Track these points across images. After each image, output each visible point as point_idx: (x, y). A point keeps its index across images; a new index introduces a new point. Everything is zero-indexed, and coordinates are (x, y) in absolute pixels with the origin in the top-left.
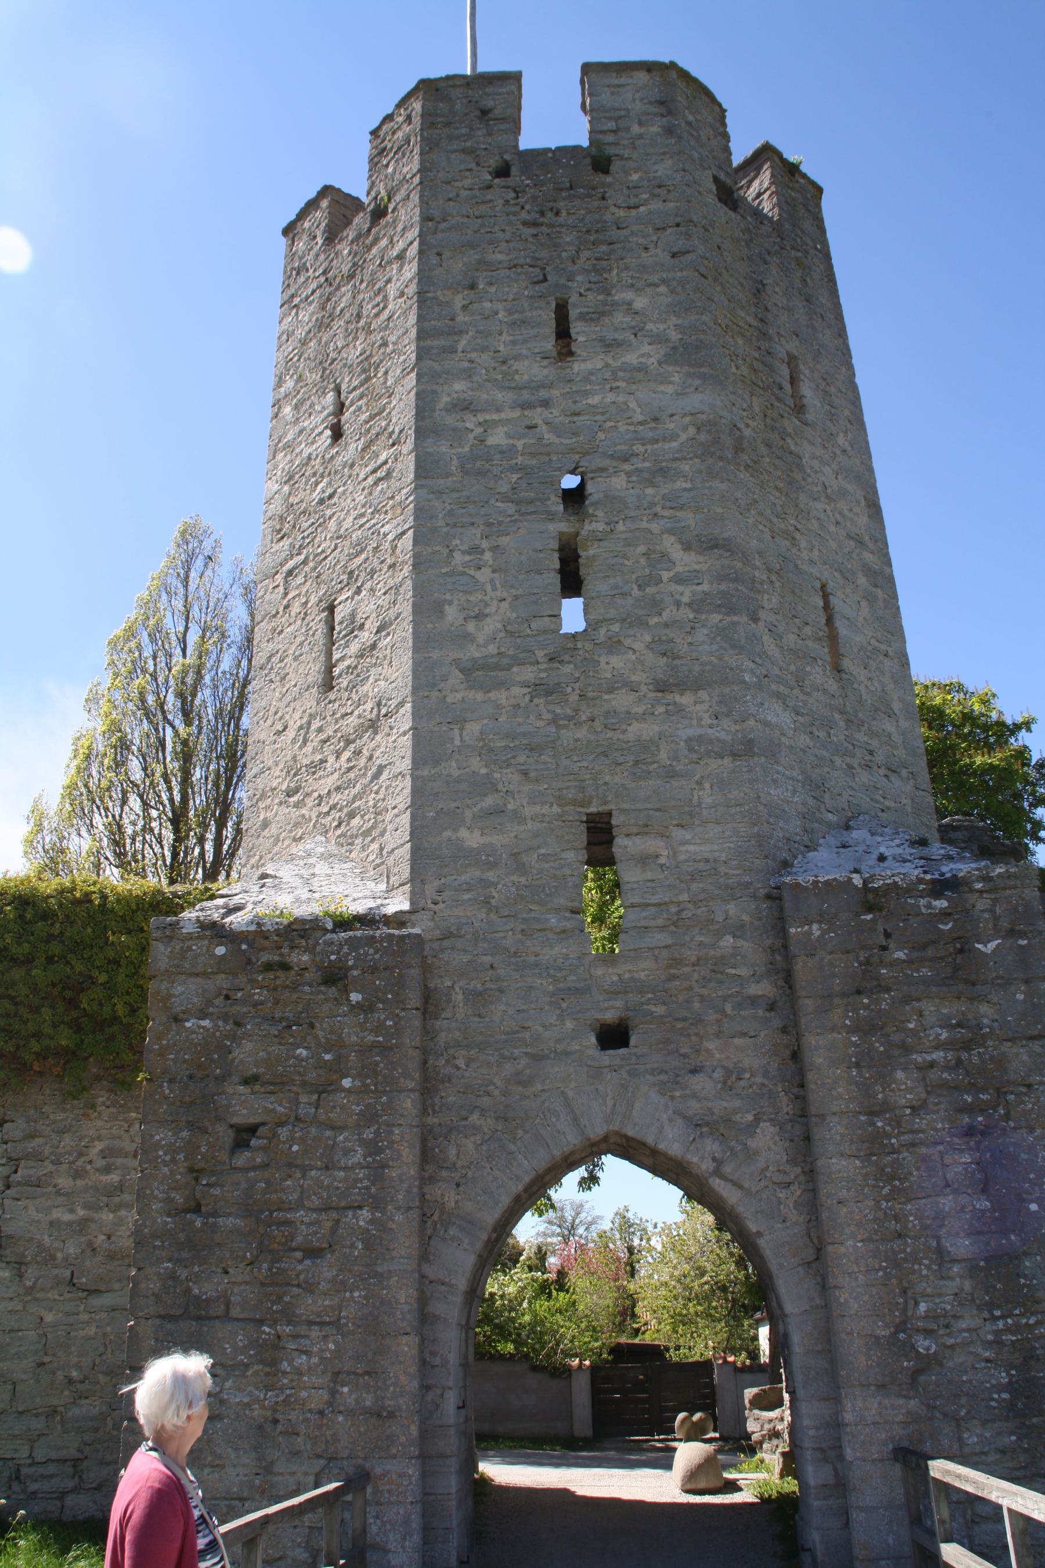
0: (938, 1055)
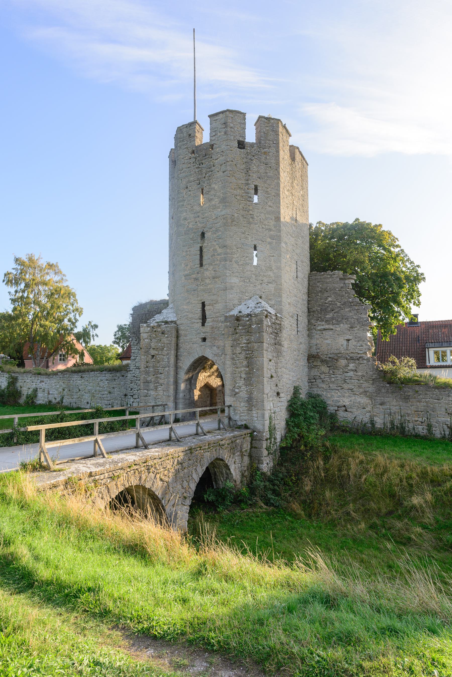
0: (244, 345)
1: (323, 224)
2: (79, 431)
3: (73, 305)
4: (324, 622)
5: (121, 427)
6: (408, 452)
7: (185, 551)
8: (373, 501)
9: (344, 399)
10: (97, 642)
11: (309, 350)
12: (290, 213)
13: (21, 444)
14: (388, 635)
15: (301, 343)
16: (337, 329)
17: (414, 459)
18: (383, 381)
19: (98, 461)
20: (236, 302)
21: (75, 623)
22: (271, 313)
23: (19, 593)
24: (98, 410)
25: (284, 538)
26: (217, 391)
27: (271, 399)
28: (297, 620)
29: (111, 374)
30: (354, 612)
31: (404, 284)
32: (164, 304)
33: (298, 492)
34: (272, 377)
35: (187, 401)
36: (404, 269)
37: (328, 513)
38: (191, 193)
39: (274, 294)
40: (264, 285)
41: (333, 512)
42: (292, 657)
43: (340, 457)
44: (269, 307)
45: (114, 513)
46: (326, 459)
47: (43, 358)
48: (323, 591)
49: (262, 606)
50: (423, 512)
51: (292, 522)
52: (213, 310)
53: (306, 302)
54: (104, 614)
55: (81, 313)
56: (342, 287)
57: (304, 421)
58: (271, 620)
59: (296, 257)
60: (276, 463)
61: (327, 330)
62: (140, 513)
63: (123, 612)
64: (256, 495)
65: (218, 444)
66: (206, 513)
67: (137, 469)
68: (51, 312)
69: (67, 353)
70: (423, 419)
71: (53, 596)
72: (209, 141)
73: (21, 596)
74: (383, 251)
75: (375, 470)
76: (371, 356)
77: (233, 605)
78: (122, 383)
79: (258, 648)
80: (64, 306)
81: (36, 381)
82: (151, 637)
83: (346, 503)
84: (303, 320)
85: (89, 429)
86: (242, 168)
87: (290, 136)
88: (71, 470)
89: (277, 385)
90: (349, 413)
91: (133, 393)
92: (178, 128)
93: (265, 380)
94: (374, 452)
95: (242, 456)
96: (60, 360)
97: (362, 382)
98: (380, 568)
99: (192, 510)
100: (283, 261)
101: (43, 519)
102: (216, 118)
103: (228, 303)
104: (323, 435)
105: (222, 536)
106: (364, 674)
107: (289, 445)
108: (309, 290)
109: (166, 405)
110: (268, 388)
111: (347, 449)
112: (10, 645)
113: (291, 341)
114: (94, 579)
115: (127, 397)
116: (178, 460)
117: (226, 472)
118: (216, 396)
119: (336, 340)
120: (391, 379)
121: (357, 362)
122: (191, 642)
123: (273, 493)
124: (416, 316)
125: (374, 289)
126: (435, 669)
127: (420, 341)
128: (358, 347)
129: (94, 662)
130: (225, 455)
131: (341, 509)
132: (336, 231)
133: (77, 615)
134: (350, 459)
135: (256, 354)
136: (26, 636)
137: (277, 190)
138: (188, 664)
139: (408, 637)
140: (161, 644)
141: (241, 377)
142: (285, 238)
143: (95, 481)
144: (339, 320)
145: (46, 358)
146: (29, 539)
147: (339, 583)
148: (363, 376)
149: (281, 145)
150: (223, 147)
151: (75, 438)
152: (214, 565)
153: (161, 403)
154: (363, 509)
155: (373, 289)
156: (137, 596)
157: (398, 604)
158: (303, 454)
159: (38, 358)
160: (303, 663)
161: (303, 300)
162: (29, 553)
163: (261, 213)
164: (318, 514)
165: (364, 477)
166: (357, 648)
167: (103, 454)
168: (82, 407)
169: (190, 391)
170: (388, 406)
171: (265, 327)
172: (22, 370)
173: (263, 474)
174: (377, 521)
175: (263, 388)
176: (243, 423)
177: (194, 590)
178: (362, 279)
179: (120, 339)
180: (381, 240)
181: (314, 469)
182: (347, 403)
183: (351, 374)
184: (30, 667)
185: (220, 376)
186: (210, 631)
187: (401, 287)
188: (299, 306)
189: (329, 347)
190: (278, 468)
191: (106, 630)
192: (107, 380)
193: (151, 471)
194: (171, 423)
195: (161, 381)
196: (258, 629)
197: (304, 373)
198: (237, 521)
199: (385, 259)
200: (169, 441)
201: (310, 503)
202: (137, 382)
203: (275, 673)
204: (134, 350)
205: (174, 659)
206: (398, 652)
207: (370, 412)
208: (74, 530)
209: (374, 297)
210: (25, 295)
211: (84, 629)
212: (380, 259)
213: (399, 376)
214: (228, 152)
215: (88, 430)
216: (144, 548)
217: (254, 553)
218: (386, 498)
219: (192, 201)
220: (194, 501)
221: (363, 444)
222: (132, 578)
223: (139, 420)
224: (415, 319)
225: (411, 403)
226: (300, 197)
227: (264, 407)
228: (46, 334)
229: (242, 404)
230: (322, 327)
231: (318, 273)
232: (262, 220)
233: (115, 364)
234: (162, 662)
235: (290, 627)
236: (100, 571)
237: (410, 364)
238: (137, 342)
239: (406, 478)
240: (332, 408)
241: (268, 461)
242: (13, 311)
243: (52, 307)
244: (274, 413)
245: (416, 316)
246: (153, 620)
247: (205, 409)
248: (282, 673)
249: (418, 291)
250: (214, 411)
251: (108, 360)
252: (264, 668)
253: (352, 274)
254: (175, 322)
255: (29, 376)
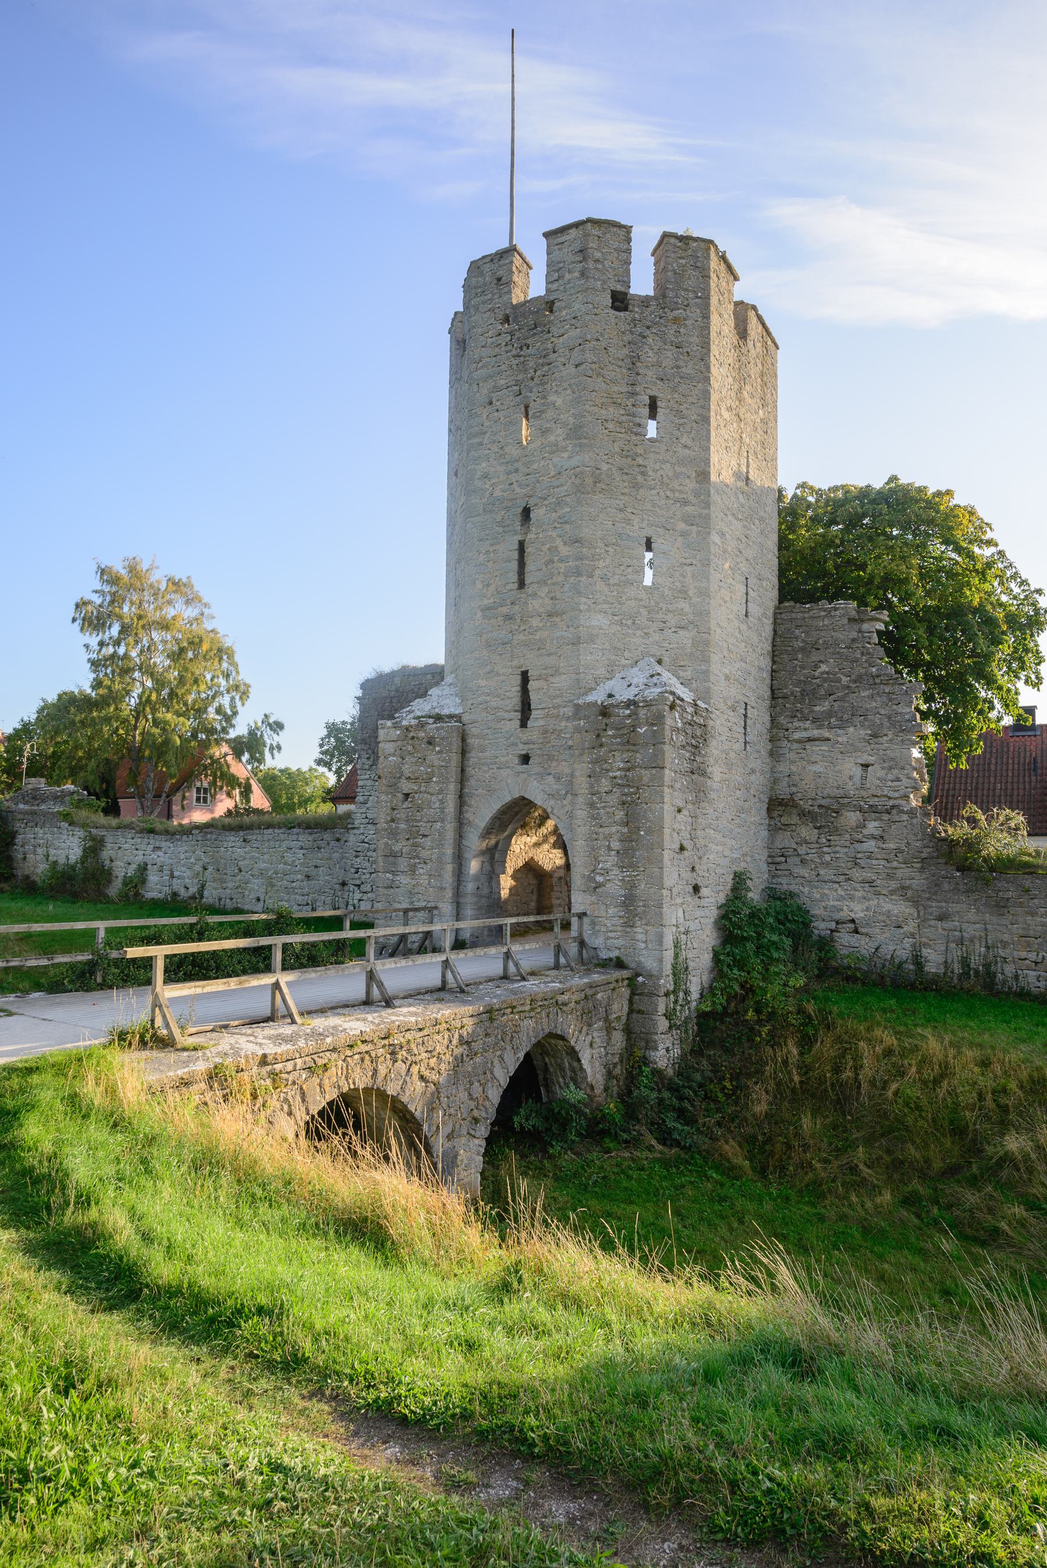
0: (618, 773)
1: (811, 488)
2: (240, 962)
3: (227, 676)
4: (786, 1407)
5: (333, 955)
6: (1000, 1031)
7: (474, 1238)
8: (914, 1143)
9: (852, 905)
10: (277, 1423)
11: (772, 788)
12: (734, 463)
13: (111, 987)
14: (933, 1442)
15: (753, 771)
16: (840, 739)
17: (1014, 1047)
18: (946, 863)
19: (281, 1031)
20: (602, 672)
21: (230, 1380)
22: (682, 700)
23: (110, 1309)
24: (280, 916)
25: (701, 1219)
26: (554, 880)
27: (679, 901)
28: (725, 1400)
29: (311, 834)
30: (856, 1389)
31: (1004, 633)
32: (433, 675)
33: (737, 1117)
34: (682, 848)
35: (484, 900)
36: (1004, 598)
37: (805, 1166)
38: (501, 414)
39: (692, 654)
40: (668, 633)
41: (818, 1165)
42: (709, 1478)
43: (838, 1039)
44: (679, 686)
45: (316, 1147)
46: (806, 1042)
47: (160, 796)
48: (786, 1339)
49: (644, 1366)
50: (1030, 1171)
51: (722, 1185)
52: (548, 690)
53: (766, 675)
54: (292, 1365)
55: (245, 695)
56: (854, 640)
57: (757, 954)
58: (665, 1397)
59: (744, 567)
60: (688, 1048)
61: (815, 740)
62: (374, 1150)
63: (335, 1362)
64: (638, 1121)
65: (554, 1001)
66: (523, 1156)
67: (367, 1052)
68: (180, 692)
69: (213, 783)
70: (1040, 956)
71: (182, 1320)
72: (543, 293)
73: (114, 1317)
74: (953, 555)
75: (919, 1072)
76: (920, 804)
77: (580, 1361)
78: (336, 855)
79: (634, 1455)
80: (209, 677)
81: (144, 847)
82: (394, 1419)
83: (850, 1146)
84: (760, 716)
85: (261, 959)
86: (621, 357)
87: (736, 279)
88: (220, 1048)
89: (693, 868)
90: (863, 937)
91: (359, 878)
92: (472, 263)
93: (667, 855)
94: (919, 1030)
95: (609, 1029)
96: (198, 799)
97: (895, 864)
98: (923, 1294)
99: (492, 1148)
100: (715, 576)
101: (159, 1156)
102: (561, 240)
103: (582, 675)
104: (801, 987)
105: (559, 1209)
106: (874, 1523)
107: (719, 1008)
108: (774, 646)
109: (436, 908)
110: (673, 875)
111: (855, 1021)
112: (90, 1418)
113: (730, 766)
114: (271, 1288)
115: (346, 888)
116: (461, 1036)
117: (570, 1065)
118: (552, 890)
119: (834, 764)
120: (967, 859)
121: (886, 817)
122: (482, 1436)
123: (679, 1117)
124: (1031, 711)
125: (930, 645)
126: (1037, 1521)
127: (1039, 771)
128: (890, 783)
129: (269, 1464)
130: (570, 1027)
131: (836, 1157)
132: (843, 505)
133: (233, 1363)
134: (862, 1044)
135: (645, 794)
136: (126, 1400)
137: (703, 407)
138: (475, 1480)
139: (980, 1447)
140: (417, 1435)
141: (609, 848)
142: (720, 521)
143: (274, 1075)
144: (846, 717)
145: (167, 797)
146: (129, 1195)
147: (825, 1322)
148: (898, 850)
149: (714, 301)
150: (577, 306)
151: (230, 976)
152: (540, 1271)
153: (424, 904)
154: (887, 1159)
155: (927, 643)
156: (367, 1330)
157: (961, 1375)
158: (752, 1029)
159: (150, 796)
160: (735, 1493)
161: (760, 669)
162: (129, 1225)
163: (664, 462)
164: (783, 1168)
165: (894, 1086)
166: (861, 1466)
167: (291, 1016)
168: (246, 907)
169: (491, 878)
170: (957, 923)
171: (667, 733)
172: (114, 822)
173: (657, 1072)
174: (921, 1189)
175: (662, 874)
176: (614, 954)
177: (491, 1325)
178: (903, 620)
179: (332, 756)
180: (951, 528)
181: (776, 1065)
182: (859, 914)
183: (871, 845)
184: (133, 1466)
185: (561, 844)
186: (527, 1412)
187: (996, 641)
188: (750, 682)
189: (820, 781)
190: (692, 1061)
191: (296, 1400)
192: (302, 848)
193: (399, 1057)
194: (445, 951)
195: (424, 854)
196: (635, 1415)
197: (759, 842)
198: (594, 1177)
199: (958, 574)
200: (441, 992)
201: (765, 1143)
202: (368, 854)
203: (670, 1510)
204: (364, 780)
205: (445, 1468)
206: (955, 1481)
207: (913, 936)
208: (226, 1179)
209: (929, 665)
210: (121, 651)
211: (249, 1393)
212: (947, 573)
213: (984, 853)
214: (588, 318)
215: (257, 961)
216: (381, 1227)
217: (631, 1250)
218: (944, 1135)
219: (503, 433)
220: (496, 1128)
221: (893, 1011)
222: (355, 1291)
223: (373, 941)
224: (1026, 720)
225: (1011, 917)
226: (759, 425)
227: (662, 918)
228: (167, 742)
229: (611, 911)
230: (805, 734)
231: (798, 605)
232: (665, 479)
233: (319, 810)
234: (419, 1473)
235: (708, 1413)
236: (284, 1272)
237: (1013, 825)
238: (370, 763)
239: (994, 1092)
240: (822, 925)
241: (669, 1044)
242: (93, 688)
243: (181, 680)
244: (686, 933)
245: (1031, 711)
246: (400, 1382)
247: (525, 919)
248: (687, 1511)
249: (1037, 651)
250: (547, 925)
251: (305, 802)
252: (645, 1500)
253: (880, 607)
254: (457, 718)
255: (130, 836)
